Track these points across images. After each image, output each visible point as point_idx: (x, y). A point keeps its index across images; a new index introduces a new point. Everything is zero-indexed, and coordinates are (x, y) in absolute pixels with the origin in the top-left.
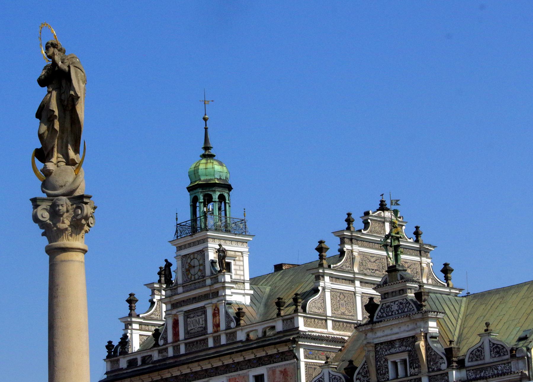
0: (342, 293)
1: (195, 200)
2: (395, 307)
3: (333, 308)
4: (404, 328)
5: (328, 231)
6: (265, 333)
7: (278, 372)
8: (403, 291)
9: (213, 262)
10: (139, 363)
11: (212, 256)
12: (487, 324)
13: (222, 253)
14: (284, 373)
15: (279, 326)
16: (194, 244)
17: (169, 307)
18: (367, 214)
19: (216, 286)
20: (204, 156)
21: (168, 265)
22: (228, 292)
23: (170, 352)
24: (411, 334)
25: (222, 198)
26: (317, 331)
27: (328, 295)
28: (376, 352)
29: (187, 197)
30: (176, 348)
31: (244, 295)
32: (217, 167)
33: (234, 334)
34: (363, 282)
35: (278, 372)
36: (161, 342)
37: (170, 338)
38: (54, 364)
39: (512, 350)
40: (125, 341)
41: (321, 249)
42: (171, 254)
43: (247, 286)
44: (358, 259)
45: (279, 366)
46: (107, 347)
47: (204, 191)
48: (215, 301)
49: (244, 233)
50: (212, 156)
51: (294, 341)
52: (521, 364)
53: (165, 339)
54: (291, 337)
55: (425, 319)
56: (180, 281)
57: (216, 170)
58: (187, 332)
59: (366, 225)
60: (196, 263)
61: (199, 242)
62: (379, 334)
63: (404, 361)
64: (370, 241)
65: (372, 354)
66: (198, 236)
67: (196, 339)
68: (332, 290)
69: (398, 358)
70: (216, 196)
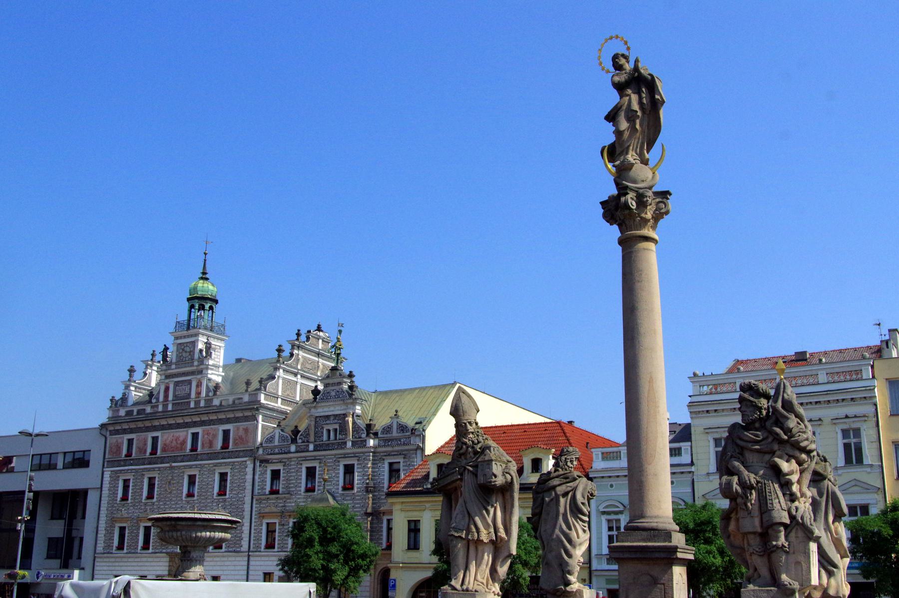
0: (289, 381)
1: (192, 307)
2: (333, 394)
3: (283, 391)
4: (338, 408)
5: (285, 338)
6: (234, 402)
7: (241, 429)
8: (340, 383)
9: (201, 351)
10: (135, 413)
11: (201, 346)
12: (396, 411)
13: (208, 346)
14: (246, 430)
15: (246, 398)
16: (188, 336)
17: (163, 377)
18: (309, 332)
19: (202, 367)
20: (202, 278)
21: (166, 349)
22: (210, 372)
23: (160, 408)
24: (343, 412)
25: (211, 308)
26: (272, 404)
27: (281, 381)
28: (316, 422)
29: (187, 305)
30: (165, 406)
31: (218, 375)
32: (211, 287)
33: (211, 400)
34: (303, 377)
35: (241, 429)
36: (154, 401)
37: (161, 398)
38: (631, 274)
39: (412, 429)
40: (124, 399)
41: (280, 350)
42: (170, 342)
43: (221, 369)
44: (301, 360)
45: (243, 425)
46: (111, 400)
47: (200, 302)
48: (199, 377)
49: (223, 334)
50: (207, 279)
51: (257, 409)
52: (417, 439)
53: (158, 399)
54: (254, 407)
55: (354, 404)
56: (174, 361)
57: (208, 288)
59: (308, 339)
60: (188, 349)
61: (192, 336)
62: (320, 410)
63: (336, 430)
64: (310, 350)
65: (313, 423)
66: (192, 331)
67: (182, 402)
68: (284, 379)
69: (331, 427)
70: (207, 306)
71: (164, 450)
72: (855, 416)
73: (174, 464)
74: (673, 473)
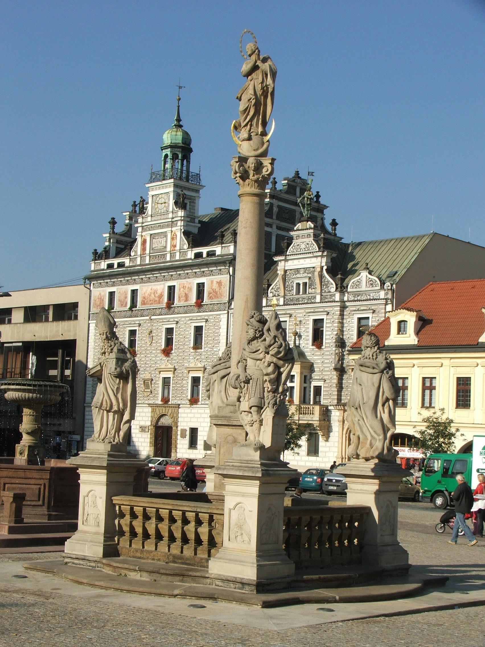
7: (215, 283)
34: (279, 228)
35: (215, 283)
62: (290, 262)
63: (305, 284)
71: (143, 303)
73: (153, 317)
74: (223, 510)
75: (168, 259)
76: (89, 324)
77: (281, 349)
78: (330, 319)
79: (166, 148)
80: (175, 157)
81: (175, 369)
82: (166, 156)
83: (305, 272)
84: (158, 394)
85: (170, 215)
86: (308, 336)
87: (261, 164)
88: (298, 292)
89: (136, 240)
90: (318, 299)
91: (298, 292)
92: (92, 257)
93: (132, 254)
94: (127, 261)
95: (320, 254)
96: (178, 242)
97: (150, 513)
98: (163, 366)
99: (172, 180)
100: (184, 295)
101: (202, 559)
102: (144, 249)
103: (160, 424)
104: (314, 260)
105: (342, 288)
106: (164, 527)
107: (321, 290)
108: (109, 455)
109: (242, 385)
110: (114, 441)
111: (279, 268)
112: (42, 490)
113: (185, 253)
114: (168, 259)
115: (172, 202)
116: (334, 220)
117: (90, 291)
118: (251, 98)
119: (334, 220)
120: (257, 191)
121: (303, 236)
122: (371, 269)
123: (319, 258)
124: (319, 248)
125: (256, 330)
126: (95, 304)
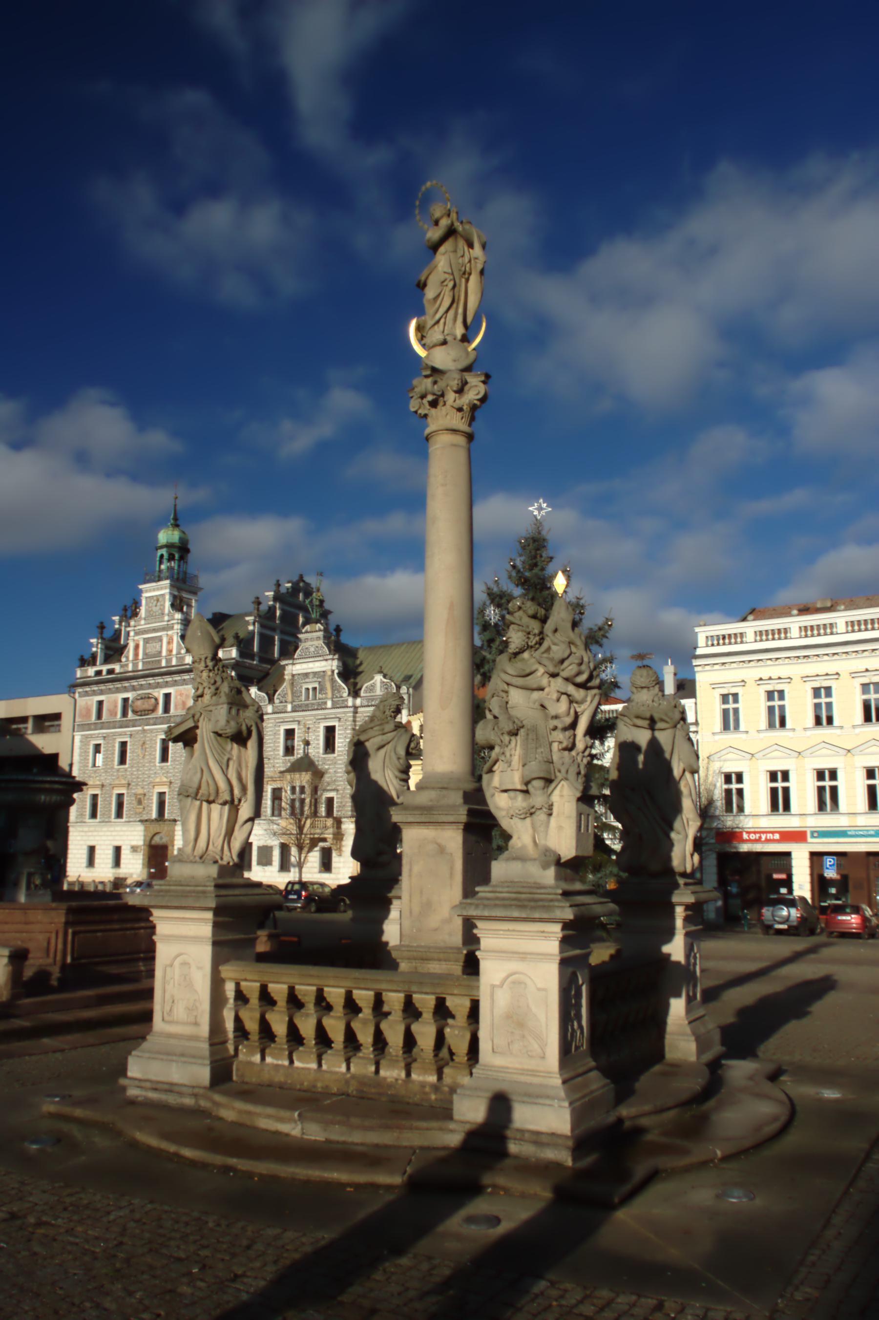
58: (145, 654)
62: (298, 667)
63: (315, 689)
72: (818, 675)
73: (146, 728)
75: (164, 664)
76: (73, 737)
77: (583, 667)
78: (342, 726)
79: (162, 547)
80: (171, 558)
81: (171, 783)
82: (162, 556)
83: (314, 677)
84: (151, 810)
85: (166, 618)
86: (318, 744)
87: (466, 383)
88: (307, 698)
89: (125, 646)
90: (329, 704)
91: (307, 698)
92: (78, 663)
93: (123, 659)
94: (117, 668)
95: (331, 657)
96: (174, 646)
97: (305, 995)
98: (158, 780)
99: (168, 582)
100: (180, 702)
101: (423, 1085)
102: (136, 655)
103: (153, 842)
104: (324, 663)
105: (355, 693)
106: (335, 1027)
107: (333, 695)
108: (217, 886)
109: (506, 738)
110: (222, 859)
111: (286, 672)
112: (53, 941)
113: (183, 658)
114: (164, 664)
115: (168, 604)
116: (338, 626)
117: (75, 700)
118: (446, 280)
119: (338, 626)
120: (463, 426)
121: (312, 637)
122: (385, 672)
123: (330, 662)
124: (330, 651)
125: (529, 633)
126: (81, 710)
